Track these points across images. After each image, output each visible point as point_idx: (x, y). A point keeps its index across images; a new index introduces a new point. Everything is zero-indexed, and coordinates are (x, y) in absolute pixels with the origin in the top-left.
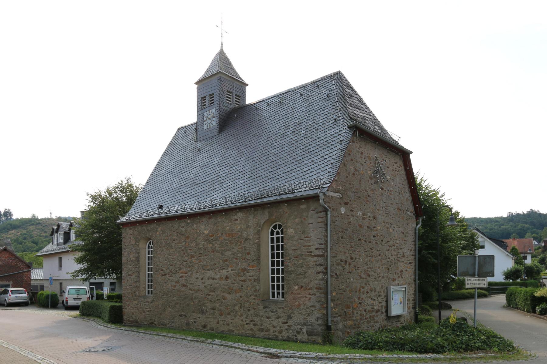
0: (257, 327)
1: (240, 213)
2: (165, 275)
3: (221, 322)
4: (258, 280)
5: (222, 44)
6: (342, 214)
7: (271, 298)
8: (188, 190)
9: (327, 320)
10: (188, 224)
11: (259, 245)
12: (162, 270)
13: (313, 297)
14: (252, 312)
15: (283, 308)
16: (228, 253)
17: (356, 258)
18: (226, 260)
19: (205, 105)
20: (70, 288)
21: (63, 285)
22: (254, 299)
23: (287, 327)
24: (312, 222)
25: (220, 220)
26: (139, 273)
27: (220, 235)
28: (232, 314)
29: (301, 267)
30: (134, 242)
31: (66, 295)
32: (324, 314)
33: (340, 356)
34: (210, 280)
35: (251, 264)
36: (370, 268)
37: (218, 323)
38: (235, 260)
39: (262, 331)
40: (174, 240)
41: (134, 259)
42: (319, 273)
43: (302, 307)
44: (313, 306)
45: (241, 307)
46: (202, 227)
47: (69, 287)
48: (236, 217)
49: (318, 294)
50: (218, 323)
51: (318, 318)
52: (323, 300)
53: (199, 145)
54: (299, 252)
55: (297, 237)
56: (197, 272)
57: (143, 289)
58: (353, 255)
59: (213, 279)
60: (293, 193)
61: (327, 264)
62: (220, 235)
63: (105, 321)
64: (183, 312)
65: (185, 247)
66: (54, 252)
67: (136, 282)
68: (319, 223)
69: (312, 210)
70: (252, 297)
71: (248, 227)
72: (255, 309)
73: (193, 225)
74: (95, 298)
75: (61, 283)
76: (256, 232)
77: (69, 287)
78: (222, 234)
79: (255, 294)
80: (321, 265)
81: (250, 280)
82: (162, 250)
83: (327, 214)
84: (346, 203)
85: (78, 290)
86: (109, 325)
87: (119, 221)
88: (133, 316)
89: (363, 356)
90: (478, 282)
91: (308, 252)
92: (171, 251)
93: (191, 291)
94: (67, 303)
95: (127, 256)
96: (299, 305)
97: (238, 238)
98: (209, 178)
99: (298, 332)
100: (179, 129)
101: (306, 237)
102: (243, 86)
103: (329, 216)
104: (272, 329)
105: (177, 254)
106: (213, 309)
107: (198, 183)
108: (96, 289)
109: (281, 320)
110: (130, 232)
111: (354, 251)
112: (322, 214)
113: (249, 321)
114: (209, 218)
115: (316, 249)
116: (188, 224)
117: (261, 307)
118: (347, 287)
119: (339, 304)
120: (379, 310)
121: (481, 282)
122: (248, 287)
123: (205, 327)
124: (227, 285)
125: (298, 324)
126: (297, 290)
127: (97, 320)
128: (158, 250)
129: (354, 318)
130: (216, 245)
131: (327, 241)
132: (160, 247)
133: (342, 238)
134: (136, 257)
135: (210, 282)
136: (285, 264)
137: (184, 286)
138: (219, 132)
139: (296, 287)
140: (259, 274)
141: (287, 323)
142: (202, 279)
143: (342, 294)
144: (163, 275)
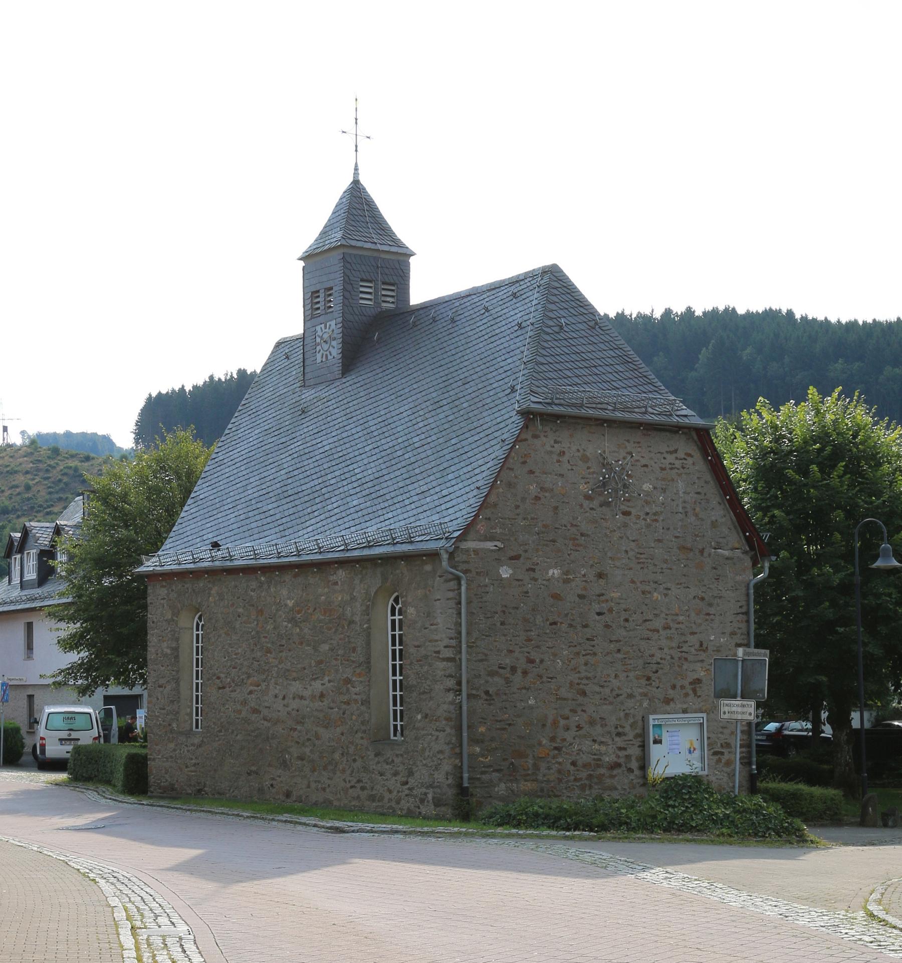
0: (366, 792)
1: (341, 571)
2: (224, 688)
3: (313, 785)
4: (366, 702)
5: (356, 169)
6: (502, 579)
7: (392, 737)
8: (270, 507)
9: (461, 778)
10: (262, 584)
11: (369, 635)
12: (218, 678)
13: (441, 735)
14: (359, 763)
15: (402, 755)
16: (325, 647)
17: (542, 661)
18: (321, 662)
19: (318, 308)
20: (53, 709)
21: (36, 701)
22: (362, 738)
23: (407, 792)
24: (439, 597)
25: (311, 580)
26: (177, 681)
27: (310, 611)
28: (330, 767)
29: (426, 679)
30: (169, 616)
31: (42, 731)
32: (455, 766)
33: (419, 829)
34: (297, 700)
35: (358, 671)
36: (588, 678)
37: (309, 787)
38: (334, 662)
39: (374, 801)
40: (239, 616)
41: (169, 651)
42: (449, 690)
43: (427, 753)
44: (440, 752)
45: (342, 754)
46: (284, 592)
47: (48, 710)
48: (335, 577)
49: (448, 730)
50: (309, 787)
51: (447, 774)
52: (454, 739)
53: (309, 395)
54: (423, 651)
55: (419, 625)
56: (276, 684)
57: (187, 718)
58: (534, 655)
59: (302, 698)
60: (412, 542)
61: (461, 675)
62: (310, 611)
63: (117, 792)
64: (253, 765)
65: (258, 632)
66: (12, 608)
67: (172, 702)
68: (448, 599)
69: (440, 577)
70: (360, 735)
71: (353, 599)
72: (362, 758)
73: (269, 587)
74: (114, 740)
75: (31, 697)
76: (364, 608)
77: (48, 710)
78: (315, 609)
79: (363, 728)
80: (452, 676)
81: (356, 701)
82: (219, 636)
83: (460, 584)
84: (516, 558)
85: (70, 717)
86: (121, 797)
87: (141, 569)
88: (167, 776)
89: (456, 829)
90: (739, 709)
91: (435, 652)
92: (234, 637)
93: (265, 723)
94: (43, 751)
95: (157, 644)
96: (424, 750)
97: (339, 618)
98: (308, 486)
99: (422, 801)
100: (279, 344)
101: (432, 625)
102: (401, 258)
103: (463, 588)
104: (387, 796)
105: (244, 645)
106: (301, 758)
107: (290, 493)
108: (119, 716)
109: (398, 778)
110: (163, 592)
111: (538, 647)
112: (453, 585)
113: (355, 780)
114: (295, 576)
115: (445, 647)
116: (262, 584)
117: (371, 754)
118: (519, 716)
119: (496, 748)
120: (618, 765)
121: (745, 709)
122: (352, 714)
123: (288, 795)
124: (321, 711)
125: (422, 785)
126: (421, 721)
127: (102, 788)
128: (211, 635)
129: (540, 778)
130: (306, 630)
131: (460, 633)
132: (215, 629)
133: (502, 623)
134: (172, 649)
135: (295, 704)
136: (404, 672)
137: (255, 711)
138: (343, 374)
139: (419, 717)
140: (369, 690)
141: (407, 783)
142: (284, 698)
143: (504, 729)
144: (220, 688)
